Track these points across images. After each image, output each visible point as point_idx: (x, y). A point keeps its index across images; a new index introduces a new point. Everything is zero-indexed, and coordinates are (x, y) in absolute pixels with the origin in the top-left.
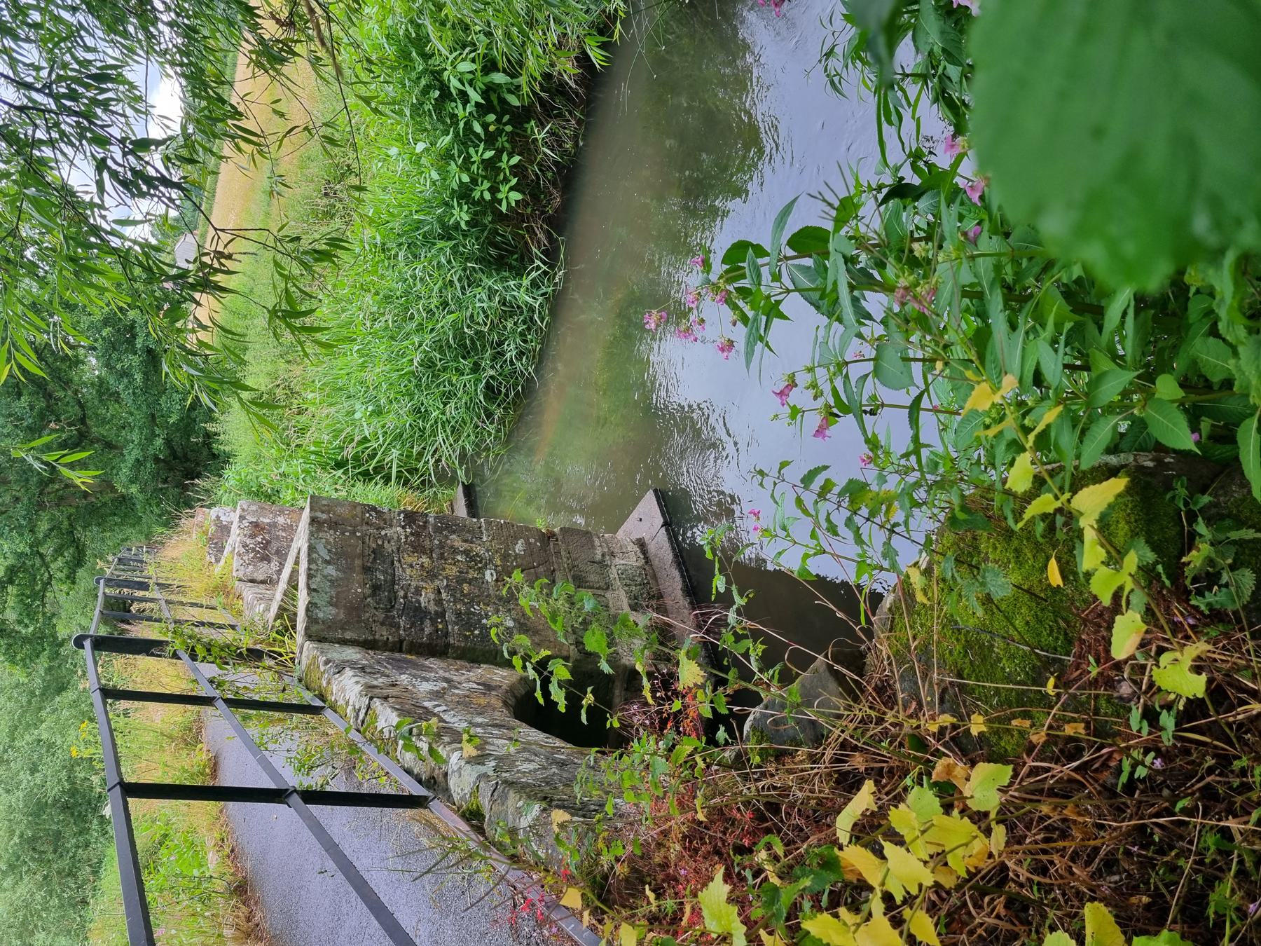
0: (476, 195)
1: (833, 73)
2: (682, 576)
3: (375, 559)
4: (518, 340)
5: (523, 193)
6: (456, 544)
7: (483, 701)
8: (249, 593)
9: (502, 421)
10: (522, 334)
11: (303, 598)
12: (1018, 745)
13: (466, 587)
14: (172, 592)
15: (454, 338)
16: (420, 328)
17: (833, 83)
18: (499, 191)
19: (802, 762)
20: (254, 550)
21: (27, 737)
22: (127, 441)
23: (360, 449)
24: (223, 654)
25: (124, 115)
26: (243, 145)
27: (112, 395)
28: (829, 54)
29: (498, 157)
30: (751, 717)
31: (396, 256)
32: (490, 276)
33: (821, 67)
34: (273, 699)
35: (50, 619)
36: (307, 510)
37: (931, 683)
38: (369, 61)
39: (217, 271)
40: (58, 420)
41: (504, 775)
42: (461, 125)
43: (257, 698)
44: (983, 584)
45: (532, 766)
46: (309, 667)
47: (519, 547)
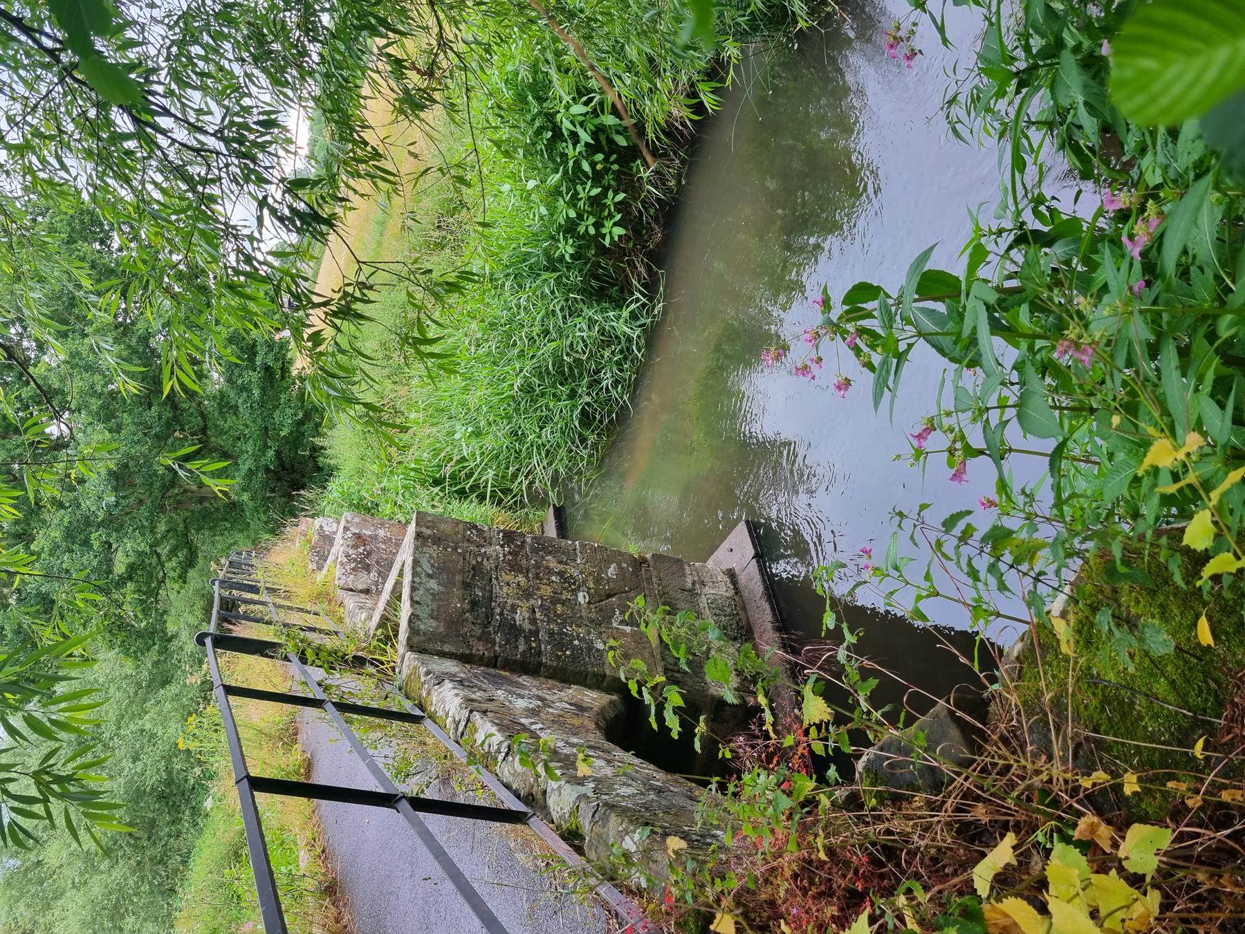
0: (582, 229)
1: (955, 119)
2: (772, 609)
3: (474, 576)
4: (615, 369)
5: (626, 228)
6: (552, 565)
7: (577, 722)
8: (350, 601)
9: (595, 446)
10: (618, 363)
11: (405, 610)
12: (1161, 808)
13: (559, 607)
14: (279, 596)
15: (554, 365)
16: (522, 354)
17: (955, 130)
18: (603, 226)
19: (920, 808)
20: (355, 560)
21: (132, 726)
22: (242, 452)
23: (457, 468)
24: (331, 659)
25: (276, 155)
26: (380, 183)
27: (231, 407)
28: (950, 103)
29: (604, 194)
30: (864, 758)
31: (503, 285)
32: (590, 307)
33: (943, 114)
34: (374, 705)
35: (162, 615)
36: (413, 524)
37: (1065, 740)
38: (500, 107)
39: (357, 299)
40: (183, 430)
41: (604, 797)
42: (571, 164)
43: (360, 703)
44: (1141, 640)
45: (630, 791)
46: (409, 676)
47: (612, 571)
